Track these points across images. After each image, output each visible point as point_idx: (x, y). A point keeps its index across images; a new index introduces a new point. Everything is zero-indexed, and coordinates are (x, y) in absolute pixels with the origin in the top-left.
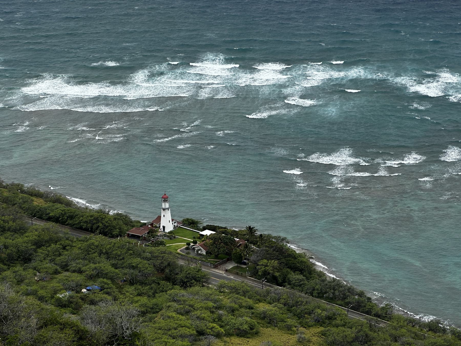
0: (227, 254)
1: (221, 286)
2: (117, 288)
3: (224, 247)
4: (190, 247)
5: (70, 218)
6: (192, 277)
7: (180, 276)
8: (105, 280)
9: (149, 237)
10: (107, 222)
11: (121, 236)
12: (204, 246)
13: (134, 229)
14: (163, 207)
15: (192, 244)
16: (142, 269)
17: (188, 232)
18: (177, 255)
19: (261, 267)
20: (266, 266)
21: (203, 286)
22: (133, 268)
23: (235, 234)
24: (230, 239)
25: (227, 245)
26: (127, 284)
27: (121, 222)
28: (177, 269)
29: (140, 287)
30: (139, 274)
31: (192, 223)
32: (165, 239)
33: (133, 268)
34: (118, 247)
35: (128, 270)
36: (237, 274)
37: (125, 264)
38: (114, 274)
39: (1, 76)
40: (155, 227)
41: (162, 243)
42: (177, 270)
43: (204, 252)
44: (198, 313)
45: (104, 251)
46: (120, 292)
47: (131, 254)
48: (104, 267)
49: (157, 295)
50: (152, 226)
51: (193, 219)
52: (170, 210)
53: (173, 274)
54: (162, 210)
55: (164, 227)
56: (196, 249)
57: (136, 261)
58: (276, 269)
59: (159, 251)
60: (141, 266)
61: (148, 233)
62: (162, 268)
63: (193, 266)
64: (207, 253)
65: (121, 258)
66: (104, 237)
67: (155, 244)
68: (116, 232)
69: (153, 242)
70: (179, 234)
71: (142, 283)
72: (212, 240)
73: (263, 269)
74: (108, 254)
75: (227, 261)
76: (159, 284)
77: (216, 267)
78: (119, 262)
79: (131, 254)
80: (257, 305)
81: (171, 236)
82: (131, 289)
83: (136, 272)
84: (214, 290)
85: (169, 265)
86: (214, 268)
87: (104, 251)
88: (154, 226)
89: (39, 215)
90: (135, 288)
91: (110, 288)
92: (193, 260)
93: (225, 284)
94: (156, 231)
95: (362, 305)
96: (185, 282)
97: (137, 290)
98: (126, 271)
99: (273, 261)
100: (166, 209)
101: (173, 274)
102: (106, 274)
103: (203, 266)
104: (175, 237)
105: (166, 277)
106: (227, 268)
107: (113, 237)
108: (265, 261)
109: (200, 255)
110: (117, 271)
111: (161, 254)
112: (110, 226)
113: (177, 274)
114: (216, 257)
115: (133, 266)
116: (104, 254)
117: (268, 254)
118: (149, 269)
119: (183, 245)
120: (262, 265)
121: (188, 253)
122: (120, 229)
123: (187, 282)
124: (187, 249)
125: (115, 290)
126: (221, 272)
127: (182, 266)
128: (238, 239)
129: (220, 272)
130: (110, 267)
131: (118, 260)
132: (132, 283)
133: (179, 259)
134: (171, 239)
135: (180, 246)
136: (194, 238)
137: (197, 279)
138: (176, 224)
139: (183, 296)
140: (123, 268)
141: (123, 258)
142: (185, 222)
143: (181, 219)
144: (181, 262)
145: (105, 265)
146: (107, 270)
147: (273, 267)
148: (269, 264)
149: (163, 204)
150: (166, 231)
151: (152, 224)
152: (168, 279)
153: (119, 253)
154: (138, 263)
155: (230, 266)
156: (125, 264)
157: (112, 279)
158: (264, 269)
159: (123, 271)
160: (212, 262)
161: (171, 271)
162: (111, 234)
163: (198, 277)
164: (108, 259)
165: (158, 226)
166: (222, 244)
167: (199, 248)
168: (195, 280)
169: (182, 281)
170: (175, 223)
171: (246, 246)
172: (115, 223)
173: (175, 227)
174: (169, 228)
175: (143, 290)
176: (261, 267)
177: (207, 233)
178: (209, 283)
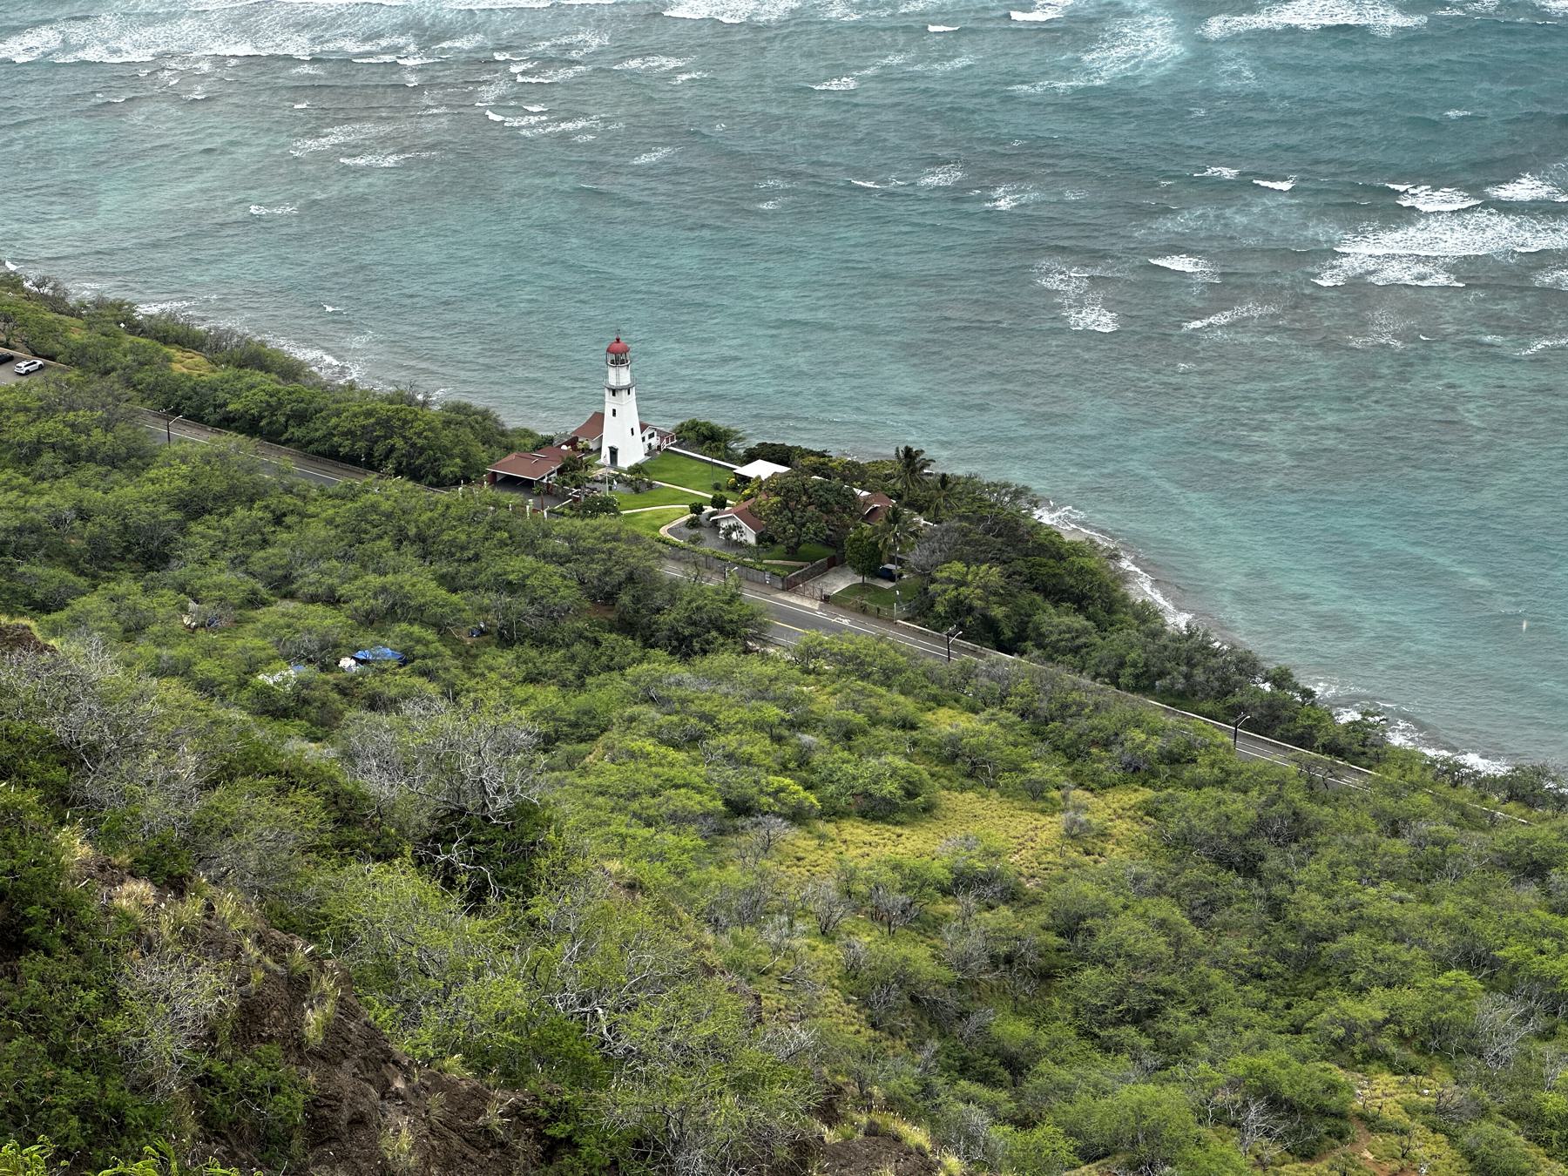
0: (828, 542)
1: (808, 653)
2: (457, 656)
3: (819, 519)
5: (291, 420)
6: (710, 621)
8: (416, 629)
9: (564, 483)
10: (419, 435)
11: (468, 481)
12: (750, 516)
13: (512, 456)
14: (612, 382)
15: (709, 509)
16: (540, 593)
18: (660, 546)
22: (511, 588)
23: (855, 473)
24: (839, 492)
26: (489, 644)
27: (466, 434)
29: (534, 653)
30: (531, 610)
31: (709, 438)
32: (619, 492)
33: (511, 588)
34: (460, 519)
35: (493, 596)
36: (863, 610)
37: (483, 577)
38: (447, 610)
41: (607, 506)
42: (659, 598)
43: (751, 538)
44: (730, 741)
45: (412, 531)
48: (414, 585)
49: (589, 680)
52: (633, 391)
54: (608, 394)
56: (724, 524)
57: (518, 565)
58: (995, 594)
60: (536, 583)
63: (713, 582)
67: (585, 507)
68: (451, 468)
69: (575, 500)
70: (667, 475)
72: (778, 494)
74: (424, 541)
76: (597, 643)
77: (790, 586)
78: (462, 569)
80: (929, 716)
81: (639, 480)
82: (504, 659)
83: (519, 604)
85: (630, 578)
87: (412, 531)
88: (580, 446)
89: (190, 407)
90: (518, 657)
91: (432, 657)
92: (711, 563)
95: (1283, 718)
96: (685, 638)
97: (525, 662)
98: (488, 599)
99: (984, 567)
101: (643, 612)
102: (420, 609)
103: (745, 584)
104: (650, 486)
105: (621, 620)
106: (827, 591)
107: (441, 483)
108: (959, 566)
110: (455, 598)
113: (658, 610)
114: (792, 553)
115: (510, 583)
116: (413, 543)
117: (967, 543)
118: (563, 592)
120: (949, 580)
121: (695, 540)
122: (466, 457)
123: (692, 636)
124: (692, 524)
125: (449, 662)
126: (807, 603)
127: (674, 584)
130: (433, 584)
132: (506, 638)
134: (637, 490)
135: (667, 516)
136: (717, 487)
137: (728, 628)
138: (655, 442)
140: (474, 588)
141: (477, 557)
142: (684, 434)
144: (672, 571)
146: (423, 596)
147: (985, 587)
148: (970, 577)
149: (612, 372)
151: (572, 442)
152: (627, 627)
154: (526, 572)
155: (838, 583)
156: (483, 577)
157: (440, 627)
159: (476, 599)
161: (637, 600)
162: (437, 474)
164: (424, 558)
165: (593, 446)
166: (812, 508)
167: (731, 523)
168: (721, 630)
169: (677, 633)
170: (651, 436)
171: (895, 517)
172: (446, 437)
173: (651, 451)
174: (633, 453)
175: (545, 663)
178: (766, 643)
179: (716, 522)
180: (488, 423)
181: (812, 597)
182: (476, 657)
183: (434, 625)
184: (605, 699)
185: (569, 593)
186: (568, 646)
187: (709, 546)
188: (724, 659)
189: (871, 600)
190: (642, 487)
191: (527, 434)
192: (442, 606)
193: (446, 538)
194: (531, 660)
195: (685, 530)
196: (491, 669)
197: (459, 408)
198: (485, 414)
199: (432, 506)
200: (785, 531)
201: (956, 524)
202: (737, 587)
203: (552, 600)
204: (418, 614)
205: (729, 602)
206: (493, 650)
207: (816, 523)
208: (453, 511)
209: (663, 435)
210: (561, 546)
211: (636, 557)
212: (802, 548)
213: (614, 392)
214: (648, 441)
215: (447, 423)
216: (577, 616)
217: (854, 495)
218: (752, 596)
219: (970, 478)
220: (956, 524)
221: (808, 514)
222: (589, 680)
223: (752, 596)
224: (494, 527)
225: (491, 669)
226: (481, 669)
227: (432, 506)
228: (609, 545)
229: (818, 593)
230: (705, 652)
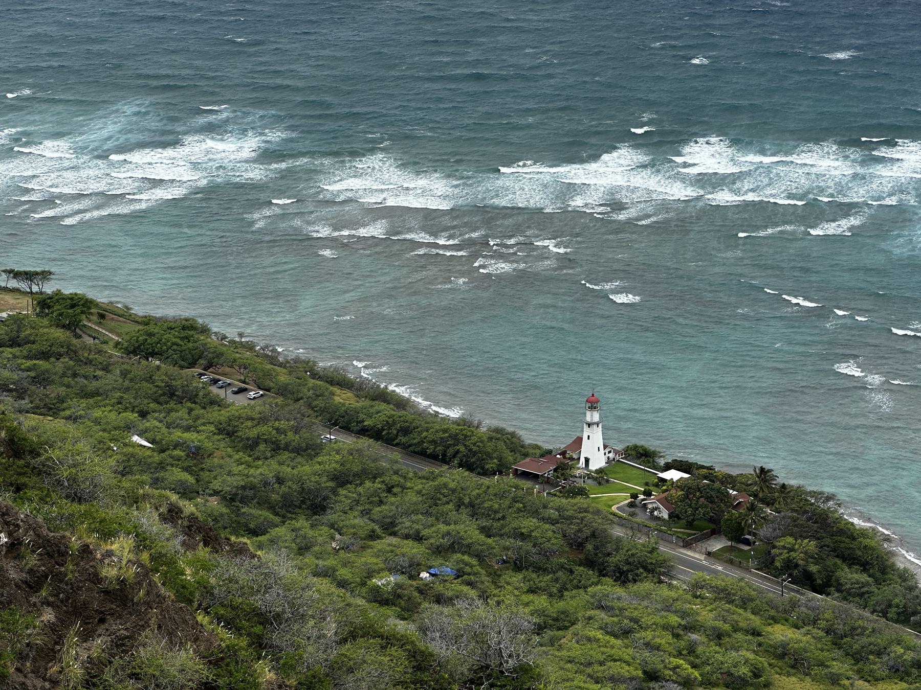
0: (711, 520)
1: (697, 586)
2: (489, 575)
3: (706, 507)
4: (637, 501)
6: (639, 563)
7: (615, 559)
8: (466, 558)
9: (558, 477)
10: (474, 444)
11: (501, 473)
12: (666, 502)
13: (528, 460)
14: (588, 419)
15: (642, 497)
16: (540, 540)
19: (781, 551)
20: (792, 550)
22: (523, 537)
23: (729, 480)
24: (718, 491)
26: (508, 569)
27: (501, 445)
28: (609, 545)
29: (534, 576)
31: (644, 455)
33: (523, 537)
34: (495, 495)
35: (512, 540)
36: (731, 562)
37: (506, 530)
38: (485, 547)
41: (582, 492)
42: (609, 548)
43: (666, 516)
45: (467, 501)
46: (494, 583)
47: (519, 510)
48: (466, 532)
49: (566, 593)
50: (564, 457)
52: (600, 426)
53: (600, 555)
54: (585, 426)
55: (587, 460)
56: (650, 506)
57: (528, 523)
58: (812, 557)
59: (576, 508)
60: (538, 535)
63: (642, 540)
64: (670, 516)
67: (569, 492)
68: (491, 465)
69: (563, 487)
70: (618, 476)
71: (539, 569)
72: (683, 490)
74: (473, 507)
76: (572, 572)
77: (687, 545)
78: (495, 524)
81: (601, 477)
82: (516, 578)
83: (528, 546)
84: (681, 592)
85: (593, 535)
86: (683, 547)
87: (467, 501)
88: (568, 456)
90: (525, 577)
91: (475, 574)
92: (642, 528)
94: (571, 468)
96: (624, 572)
97: (529, 581)
98: (509, 542)
99: (806, 541)
100: (593, 424)
101: (600, 555)
102: (469, 546)
103: (661, 542)
104: (607, 481)
105: (587, 559)
106: (710, 549)
107: (485, 473)
108: (790, 540)
109: (658, 518)
110: (490, 541)
111: (580, 512)
113: (609, 555)
114: (690, 525)
115: (522, 534)
117: (796, 526)
118: (553, 541)
119: (624, 499)
120: (784, 547)
121: (633, 515)
123: (628, 571)
124: (631, 505)
125: (484, 578)
126: (697, 556)
127: (619, 540)
129: (696, 555)
130: (477, 532)
131: (493, 519)
132: (518, 566)
133: (614, 526)
134: (600, 484)
135: (617, 500)
136: (647, 484)
137: (650, 567)
138: (611, 455)
140: (501, 535)
141: (504, 518)
142: (629, 452)
144: (618, 532)
146: (471, 538)
148: (797, 547)
149: (588, 414)
150: (590, 468)
151: (563, 453)
152: (590, 563)
154: (532, 528)
155: (717, 545)
156: (506, 530)
157: (480, 557)
158: (787, 555)
159: (502, 542)
160: (680, 535)
162: (483, 468)
163: (652, 563)
164: (473, 516)
165: (575, 456)
166: (702, 499)
167: (654, 505)
168: (645, 568)
169: (619, 568)
170: (610, 452)
171: (752, 508)
173: (609, 461)
174: (598, 462)
175: (540, 582)
176: (781, 551)
178: (672, 578)
182: (500, 576)
185: (556, 542)
188: (646, 586)
191: (537, 447)
192: (482, 545)
193: (486, 505)
195: (627, 509)
197: (498, 430)
198: (513, 435)
200: (686, 512)
202: (656, 543)
203: (547, 545)
205: (651, 552)
209: (616, 452)
210: (554, 514)
211: (597, 523)
213: (589, 425)
215: (491, 439)
216: (561, 556)
217: (728, 493)
219: (799, 487)
222: (566, 593)
225: (508, 584)
227: (479, 486)
229: (704, 550)
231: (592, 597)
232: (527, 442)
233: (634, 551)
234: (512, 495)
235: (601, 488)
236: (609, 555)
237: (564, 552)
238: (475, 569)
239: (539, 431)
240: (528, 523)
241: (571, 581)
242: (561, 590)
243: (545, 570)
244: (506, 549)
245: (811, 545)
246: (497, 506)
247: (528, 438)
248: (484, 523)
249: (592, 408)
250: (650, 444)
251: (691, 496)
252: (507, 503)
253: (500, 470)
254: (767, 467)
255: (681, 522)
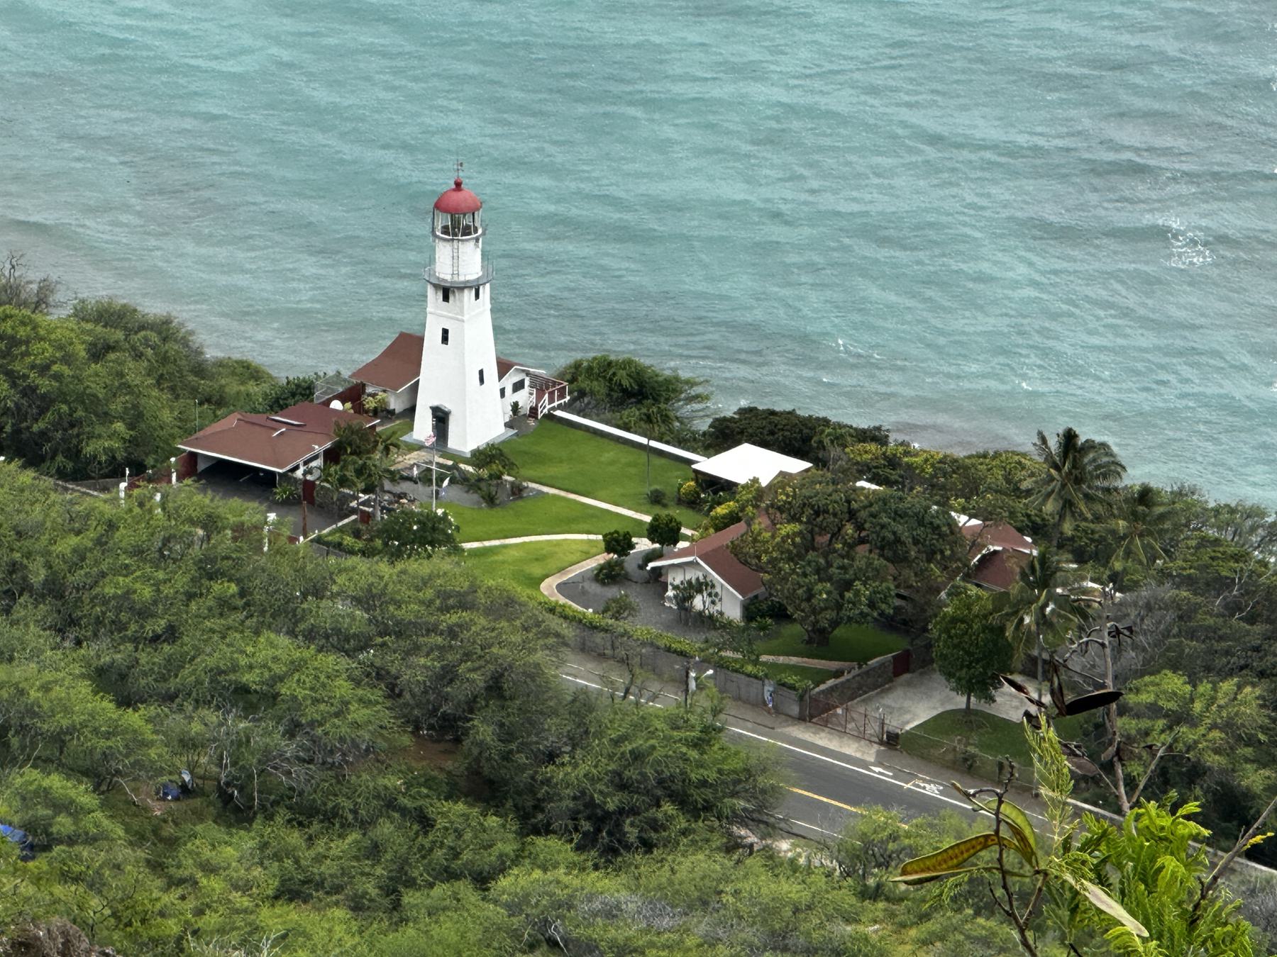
0: (892, 623)
1: (864, 858)
2: (138, 838)
3: (878, 574)
4: (630, 562)
6: (661, 782)
7: (574, 772)
8: (56, 782)
9: (343, 482)
10: (44, 369)
11: (139, 469)
12: (738, 563)
13: (232, 421)
14: (444, 270)
15: (643, 544)
16: (311, 713)
17: (610, 453)
18: (555, 623)
19: (1145, 724)
20: (1178, 718)
21: (732, 846)
22: (245, 698)
23: (957, 478)
24: (921, 519)
25: (899, 559)
26: (201, 818)
27: (135, 372)
28: (550, 722)
29: (295, 838)
30: (290, 749)
31: (633, 393)
32: (445, 503)
33: (245, 698)
34: (138, 552)
35: (213, 717)
36: (967, 766)
37: (187, 675)
38: (117, 743)
39: (1274, 246)
40: (376, 413)
41: (432, 534)
42: (553, 730)
43: (731, 606)
45: (38, 574)
46: (156, 866)
47: (225, 606)
48: (46, 688)
49: (409, 898)
50: (359, 409)
51: (645, 361)
52: (486, 292)
53: (522, 759)
54: (434, 297)
55: (441, 418)
56: (676, 578)
57: (267, 652)
58: (1251, 741)
59: (429, 593)
60: (301, 693)
61: (332, 456)
62: (446, 708)
63: (662, 702)
64: (750, 612)
65: (160, 625)
66: (28, 476)
67: (388, 533)
68: (104, 442)
69: (366, 517)
70: (553, 470)
71: (310, 814)
72: (794, 519)
73: (1161, 741)
74: (60, 596)
75: (897, 673)
76: (426, 822)
77: (815, 712)
78: (143, 658)
79: (225, 606)
81: (492, 478)
82: (233, 850)
83: (266, 735)
84: (820, 881)
85: (495, 688)
86: (802, 719)
87: (38, 574)
88: (370, 403)
90: (264, 846)
91: (91, 840)
92: (667, 662)
93: (894, 837)
94: (390, 446)
96: (608, 815)
97: (277, 857)
98: (202, 721)
99: (1227, 686)
100: (461, 288)
101: (522, 759)
102: (59, 739)
103: (731, 707)
104: (517, 491)
105: (475, 772)
106: (893, 724)
107: (81, 471)
108: (1175, 682)
109: (707, 622)
110: (134, 718)
111: (445, 609)
112: (62, 397)
113: (551, 757)
114: (819, 642)
115: (243, 690)
116: (39, 598)
117: (1192, 635)
118: (358, 713)
119: (582, 552)
120: (1154, 711)
121: (619, 609)
122: (135, 418)
123: (621, 812)
124: (608, 575)
125: (124, 853)
126: (851, 748)
127: (582, 705)
128: (974, 522)
129: (844, 748)
130: (85, 688)
131: (135, 640)
132: (235, 805)
133: (567, 654)
134: (491, 501)
135: (551, 555)
136: (656, 499)
137: (697, 796)
138: (525, 398)
139: (612, 913)
140: (170, 698)
141: (171, 634)
142: (584, 383)
143: (563, 360)
144: (578, 676)
145: (48, 676)
146: (67, 710)
147: (1228, 726)
148: (1198, 706)
149: (443, 251)
150: (453, 443)
151: (354, 394)
152: (485, 789)
153: (146, 593)
154: (279, 669)
155: (916, 708)
156: (187, 675)
157: (100, 776)
158: (1167, 738)
159: (175, 721)
160: (792, 679)
161: (507, 734)
162: (74, 454)
163: (704, 783)
164: (61, 631)
165: (396, 404)
166: (862, 550)
167: (692, 575)
168: (682, 801)
169: (591, 804)
170: (518, 386)
171: (1042, 574)
172: (96, 377)
173: (517, 417)
174: (481, 422)
175: (320, 859)
176: (1145, 724)
177: (749, 465)
178: (770, 829)
179: (658, 572)
180: (172, 348)
181: (860, 737)
182: (172, 843)
183: (86, 773)
184: (454, 938)
185: (368, 715)
186: (364, 825)
187: (645, 624)
188: (694, 865)
189: (981, 746)
190: (502, 496)
191: (249, 372)
192: (108, 735)
193: (109, 591)
194: (289, 853)
195: (595, 588)
196: (209, 869)
197: (111, 316)
198: (164, 328)
199: (76, 523)
200: (810, 596)
201: (1168, 592)
202: (716, 712)
203: (337, 728)
204: (57, 750)
205: (696, 744)
206: (208, 829)
207: (876, 584)
208: (124, 536)
209: (541, 387)
210: (337, 610)
211: (507, 644)
212: (838, 632)
213: (447, 293)
214: (511, 397)
215: (99, 352)
216: (383, 767)
217: (952, 524)
218: (747, 733)
219: (1180, 494)
220: (1168, 592)
221: (860, 563)
222: (409, 898)
223: (747, 733)
224: (209, 570)
225: (209, 869)
226: (189, 868)
227: (76, 523)
228: (452, 618)
229: (873, 729)
230: (648, 846)
231: (514, 908)
232: (211, 354)
233: (639, 743)
234: (196, 551)
235: (496, 517)
236: (551, 757)
237: (394, 751)
238: (88, 823)
239: (258, 310)
240: (267, 652)
241: (426, 853)
242: (392, 890)
243: (331, 817)
244: (188, 744)
245: (1245, 700)
246: (147, 593)
247: (217, 340)
248: (103, 651)
249: (458, 229)
250: (659, 356)
251: (823, 540)
252: (181, 581)
253: (134, 464)
254: (1085, 434)
255: (796, 629)
